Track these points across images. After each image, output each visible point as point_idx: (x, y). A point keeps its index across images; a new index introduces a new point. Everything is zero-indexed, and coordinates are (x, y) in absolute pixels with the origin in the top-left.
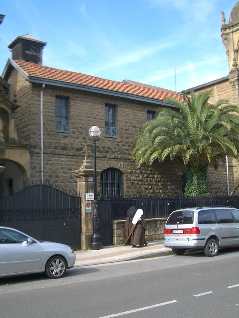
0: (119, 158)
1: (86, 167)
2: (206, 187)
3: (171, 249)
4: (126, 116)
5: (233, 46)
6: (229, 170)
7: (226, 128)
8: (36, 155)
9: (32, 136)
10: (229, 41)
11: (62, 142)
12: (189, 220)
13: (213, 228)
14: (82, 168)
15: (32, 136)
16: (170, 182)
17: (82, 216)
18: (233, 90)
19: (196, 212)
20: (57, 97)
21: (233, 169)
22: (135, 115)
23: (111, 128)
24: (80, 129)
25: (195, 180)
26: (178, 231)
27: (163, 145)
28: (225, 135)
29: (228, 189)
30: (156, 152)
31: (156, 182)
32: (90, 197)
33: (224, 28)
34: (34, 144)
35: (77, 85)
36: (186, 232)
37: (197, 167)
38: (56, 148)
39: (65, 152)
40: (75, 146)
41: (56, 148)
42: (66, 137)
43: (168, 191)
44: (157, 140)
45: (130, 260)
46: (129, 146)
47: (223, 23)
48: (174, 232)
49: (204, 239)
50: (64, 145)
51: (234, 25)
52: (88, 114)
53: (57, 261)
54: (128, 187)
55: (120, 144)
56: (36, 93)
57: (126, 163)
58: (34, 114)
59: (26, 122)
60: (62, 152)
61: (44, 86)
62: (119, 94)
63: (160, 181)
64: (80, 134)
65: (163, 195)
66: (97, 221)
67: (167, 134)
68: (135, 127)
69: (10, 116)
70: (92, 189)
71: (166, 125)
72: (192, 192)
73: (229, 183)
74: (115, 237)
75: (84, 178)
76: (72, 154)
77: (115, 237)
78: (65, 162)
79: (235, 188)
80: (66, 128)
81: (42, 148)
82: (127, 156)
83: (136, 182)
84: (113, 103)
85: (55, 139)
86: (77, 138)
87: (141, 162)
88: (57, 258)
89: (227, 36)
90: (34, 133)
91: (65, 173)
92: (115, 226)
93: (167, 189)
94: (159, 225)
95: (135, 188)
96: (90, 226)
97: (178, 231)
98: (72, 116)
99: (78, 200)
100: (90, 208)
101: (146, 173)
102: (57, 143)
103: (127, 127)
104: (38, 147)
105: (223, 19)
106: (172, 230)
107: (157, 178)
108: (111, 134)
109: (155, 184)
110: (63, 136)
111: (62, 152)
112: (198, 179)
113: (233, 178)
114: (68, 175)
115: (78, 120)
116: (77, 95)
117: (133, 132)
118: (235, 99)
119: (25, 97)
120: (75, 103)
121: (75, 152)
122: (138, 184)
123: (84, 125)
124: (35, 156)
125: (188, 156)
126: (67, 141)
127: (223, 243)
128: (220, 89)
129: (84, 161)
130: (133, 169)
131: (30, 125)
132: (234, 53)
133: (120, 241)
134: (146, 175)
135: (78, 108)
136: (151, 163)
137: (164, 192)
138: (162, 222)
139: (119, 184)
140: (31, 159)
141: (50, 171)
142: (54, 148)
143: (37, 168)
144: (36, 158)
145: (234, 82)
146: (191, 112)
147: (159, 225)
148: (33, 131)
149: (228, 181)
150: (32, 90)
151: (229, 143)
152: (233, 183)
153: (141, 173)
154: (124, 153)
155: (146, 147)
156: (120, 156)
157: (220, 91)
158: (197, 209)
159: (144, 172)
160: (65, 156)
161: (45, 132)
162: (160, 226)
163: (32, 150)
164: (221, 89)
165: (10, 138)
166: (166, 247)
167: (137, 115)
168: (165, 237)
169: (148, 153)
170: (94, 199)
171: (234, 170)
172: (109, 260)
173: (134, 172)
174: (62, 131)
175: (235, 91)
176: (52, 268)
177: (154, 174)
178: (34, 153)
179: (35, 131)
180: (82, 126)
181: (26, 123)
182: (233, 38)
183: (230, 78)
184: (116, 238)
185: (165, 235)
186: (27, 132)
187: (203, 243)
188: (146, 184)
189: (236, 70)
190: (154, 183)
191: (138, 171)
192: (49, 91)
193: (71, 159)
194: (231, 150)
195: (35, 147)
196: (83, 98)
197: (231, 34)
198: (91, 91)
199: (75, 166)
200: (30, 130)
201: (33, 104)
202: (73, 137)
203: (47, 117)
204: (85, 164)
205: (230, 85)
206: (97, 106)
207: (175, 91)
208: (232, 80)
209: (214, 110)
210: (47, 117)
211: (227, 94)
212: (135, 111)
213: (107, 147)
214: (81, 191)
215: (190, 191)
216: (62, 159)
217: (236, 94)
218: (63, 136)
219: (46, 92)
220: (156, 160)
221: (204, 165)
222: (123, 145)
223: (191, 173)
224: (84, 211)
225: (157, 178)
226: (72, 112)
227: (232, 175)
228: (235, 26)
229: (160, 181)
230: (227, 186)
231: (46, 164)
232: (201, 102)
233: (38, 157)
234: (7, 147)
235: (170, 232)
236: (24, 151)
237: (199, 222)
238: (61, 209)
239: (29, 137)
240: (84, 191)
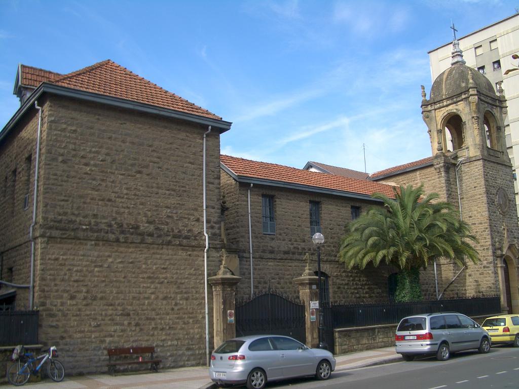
0: (325, 260)
1: (310, 275)
2: (420, 290)
3: (400, 356)
4: (330, 214)
6: (437, 269)
7: (441, 228)
8: (245, 259)
9: (241, 239)
10: (431, 120)
11: (269, 245)
12: (420, 327)
13: (444, 333)
14: (304, 276)
15: (241, 239)
16: (376, 285)
17: (306, 325)
18: (439, 178)
19: (427, 318)
20: (263, 196)
21: (441, 268)
22: (339, 212)
23: (315, 227)
24: (286, 230)
25: (408, 283)
26: (411, 338)
27: (376, 247)
28: (440, 236)
29: (437, 290)
30: (368, 254)
31: (362, 285)
32: (315, 305)
33: (425, 104)
34: (243, 248)
35: (283, 183)
36: (419, 337)
37: (410, 269)
38: (264, 251)
39: (272, 256)
40: (282, 249)
41: (264, 251)
42: (273, 239)
43: (374, 295)
44: (370, 242)
45: (367, 366)
46: (334, 247)
47: (423, 98)
48: (407, 338)
49: (436, 344)
50: (271, 248)
51: (436, 102)
52: (293, 213)
53: (325, 365)
54: (335, 292)
55: (325, 245)
56: (243, 192)
57: (332, 266)
58: (242, 215)
59: (231, 224)
60: (270, 256)
61: (252, 185)
62: (126, 103)
63: (366, 284)
64: (286, 235)
65: (369, 299)
66: (323, 329)
67: (378, 234)
68: (339, 225)
70: (316, 296)
71: (377, 224)
72: (404, 297)
73: (438, 284)
74: (336, 346)
75: (308, 286)
76: (280, 258)
77: (336, 346)
78: (272, 266)
79: (444, 289)
80: (273, 229)
81: (251, 252)
82: (333, 258)
83: (342, 286)
84: (317, 199)
85: (262, 242)
86: (284, 240)
87: (352, 263)
88: (324, 362)
89: (428, 113)
90: (242, 237)
91: (273, 279)
92: (337, 335)
93: (373, 293)
94: (376, 333)
95: (341, 293)
96: (316, 335)
97: (411, 338)
98: (278, 216)
99: (301, 308)
100: (315, 316)
101: (351, 276)
102: (265, 246)
103: (332, 225)
104: (246, 252)
105: (423, 94)
106: (404, 336)
107: (363, 281)
109: (361, 288)
110: (270, 238)
111: (270, 256)
112: (411, 282)
113: (442, 277)
114: (276, 280)
115: (284, 221)
116: (282, 193)
117: (338, 231)
118: (442, 187)
119: (230, 196)
120: (280, 201)
121: (282, 256)
122: (344, 288)
123: (289, 225)
124: (244, 261)
125: (404, 260)
126: (273, 244)
127: (454, 347)
128: (423, 176)
129: (307, 268)
130: (339, 272)
131: (238, 227)
132: (438, 133)
133: (342, 350)
134: (351, 278)
135: (283, 207)
136: (364, 267)
137: (370, 297)
138: (380, 329)
139: (325, 289)
140: (240, 264)
141: (258, 277)
142: (262, 252)
143: (247, 273)
144: (245, 263)
145: (439, 169)
146: (402, 210)
147: (376, 333)
148: (242, 234)
149: (436, 281)
150: (240, 190)
151: (445, 245)
152: (442, 284)
153: (347, 276)
154: (330, 255)
155: (356, 249)
156: (325, 258)
158: (428, 316)
159: (350, 274)
160: (272, 260)
161: (253, 235)
162: (378, 334)
163: (241, 254)
166: (398, 353)
167: (341, 212)
168: (397, 344)
169: (360, 255)
170: (318, 307)
171: (442, 269)
172: (348, 367)
173: (340, 275)
174: (269, 233)
176: (253, 383)
177: (360, 277)
178: (243, 257)
179: (244, 234)
180: (287, 226)
181: (232, 225)
183: (435, 164)
184: (337, 347)
185: (397, 342)
186: (234, 234)
187: (436, 348)
188: (352, 288)
189: (442, 155)
190: (360, 286)
191: (344, 274)
192: (256, 190)
193: (278, 263)
194: (448, 252)
195: (244, 251)
196: (288, 196)
197: (433, 111)
198: (297, 188)
200: (238, 233)
201: (241, 204)
202: (280, 239)
203: (254, 218)
204: (307, 271)
205: (435, 171)
206: (301, 203)
208: (438, 166)
209: (428, 210)
210: (254, 218)
211: (432, 181)
212: (339, 208)
213: (313, 249)
214: (305, 300)
215: (403, 295)
216: (269, 264)
217: (443, 182)
218: (270, 238)
219: (252, 191)
220: (370, 263)
221: (417, 266)
222: (329, 246)
223: (403, 275)
224: (309, 319)
225: (363, 281)
226: (277, 212)
227: (441, 274)
229: (366, 284)
230: (435, 287)
231: (255, 269)
232: (412, 198)
233: (247, 261)
235: (402, 338)
236: (233, 255)
237: (432, 328)
238: (288, 318)
239: (236, 240)
240: (308, 299)
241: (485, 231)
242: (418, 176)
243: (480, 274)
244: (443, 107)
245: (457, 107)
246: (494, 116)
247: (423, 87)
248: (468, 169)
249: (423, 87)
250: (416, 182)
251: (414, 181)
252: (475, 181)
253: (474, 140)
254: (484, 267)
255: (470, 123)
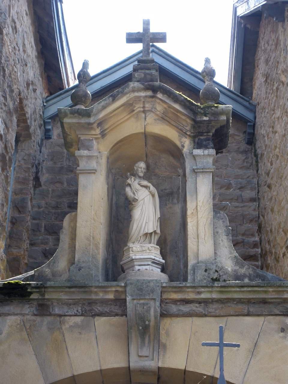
69: (189, 165)
165: (191, 262)
234: (174, 309)
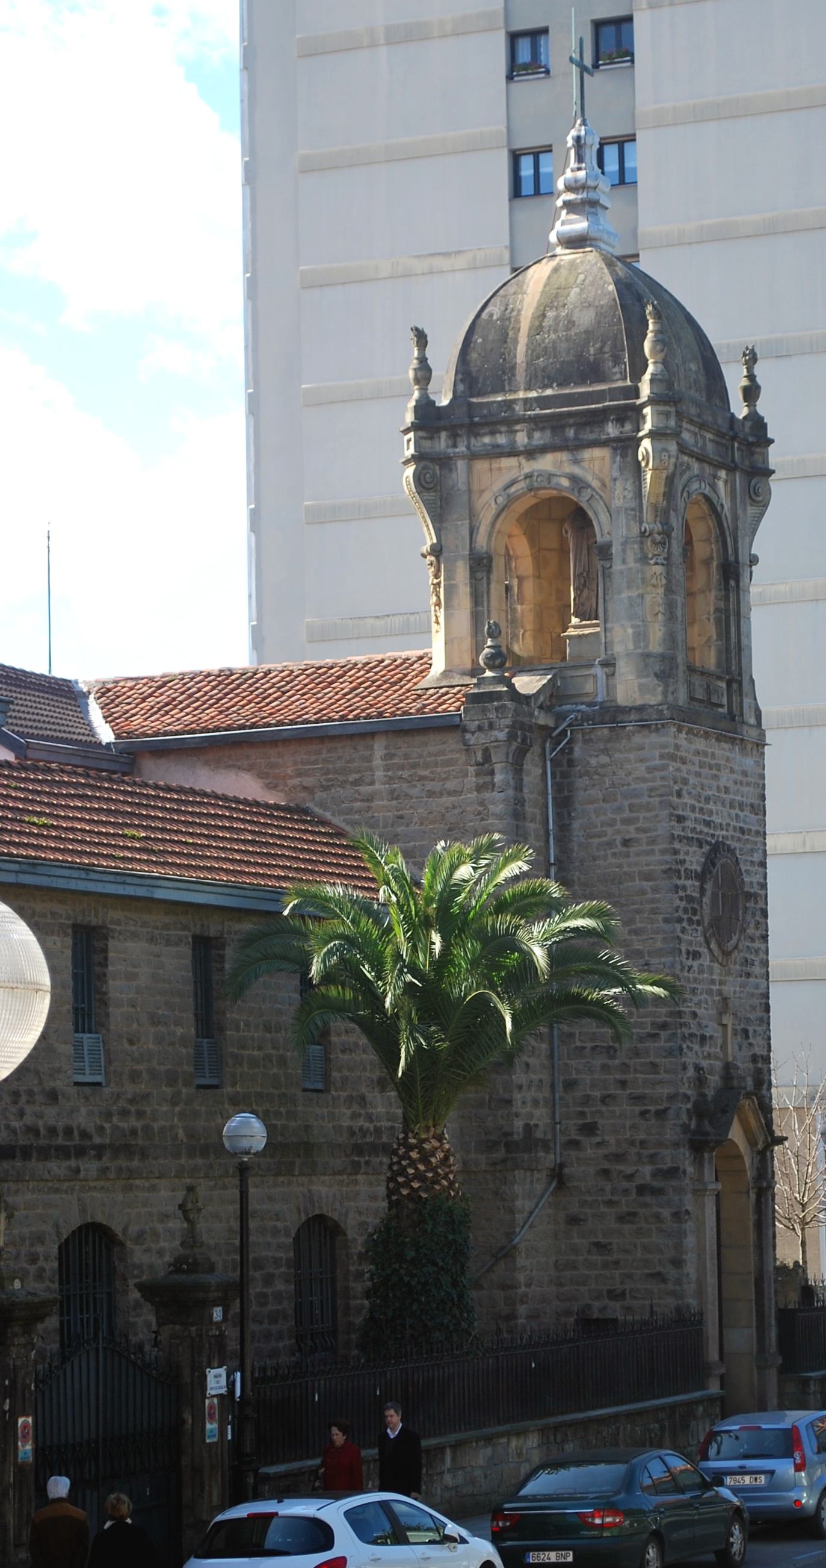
5: (466, 533)
18: (479, 789)
33: (428, 419)
108: (87, 1072)
128: (402, 767)
157: (405, 774)
164: (414, 766)
175: (487, 795)
182: (470, 491)
199: (575, 1268)
207: (47, 674)
228: (486, 430)
241: (654, 1036)
242: (377, 762)
243: (621, 1219)
244: (513, 453)
245: (576, 470)
246: (640, 475)
247: (421, 338)
248: (604, 759)
249: (421, 338)
250: (365, 789)
251: (356, 783)
252: (627, 814)
253: (641, 636)
254: (642, 1190)
255: (631, 557)
